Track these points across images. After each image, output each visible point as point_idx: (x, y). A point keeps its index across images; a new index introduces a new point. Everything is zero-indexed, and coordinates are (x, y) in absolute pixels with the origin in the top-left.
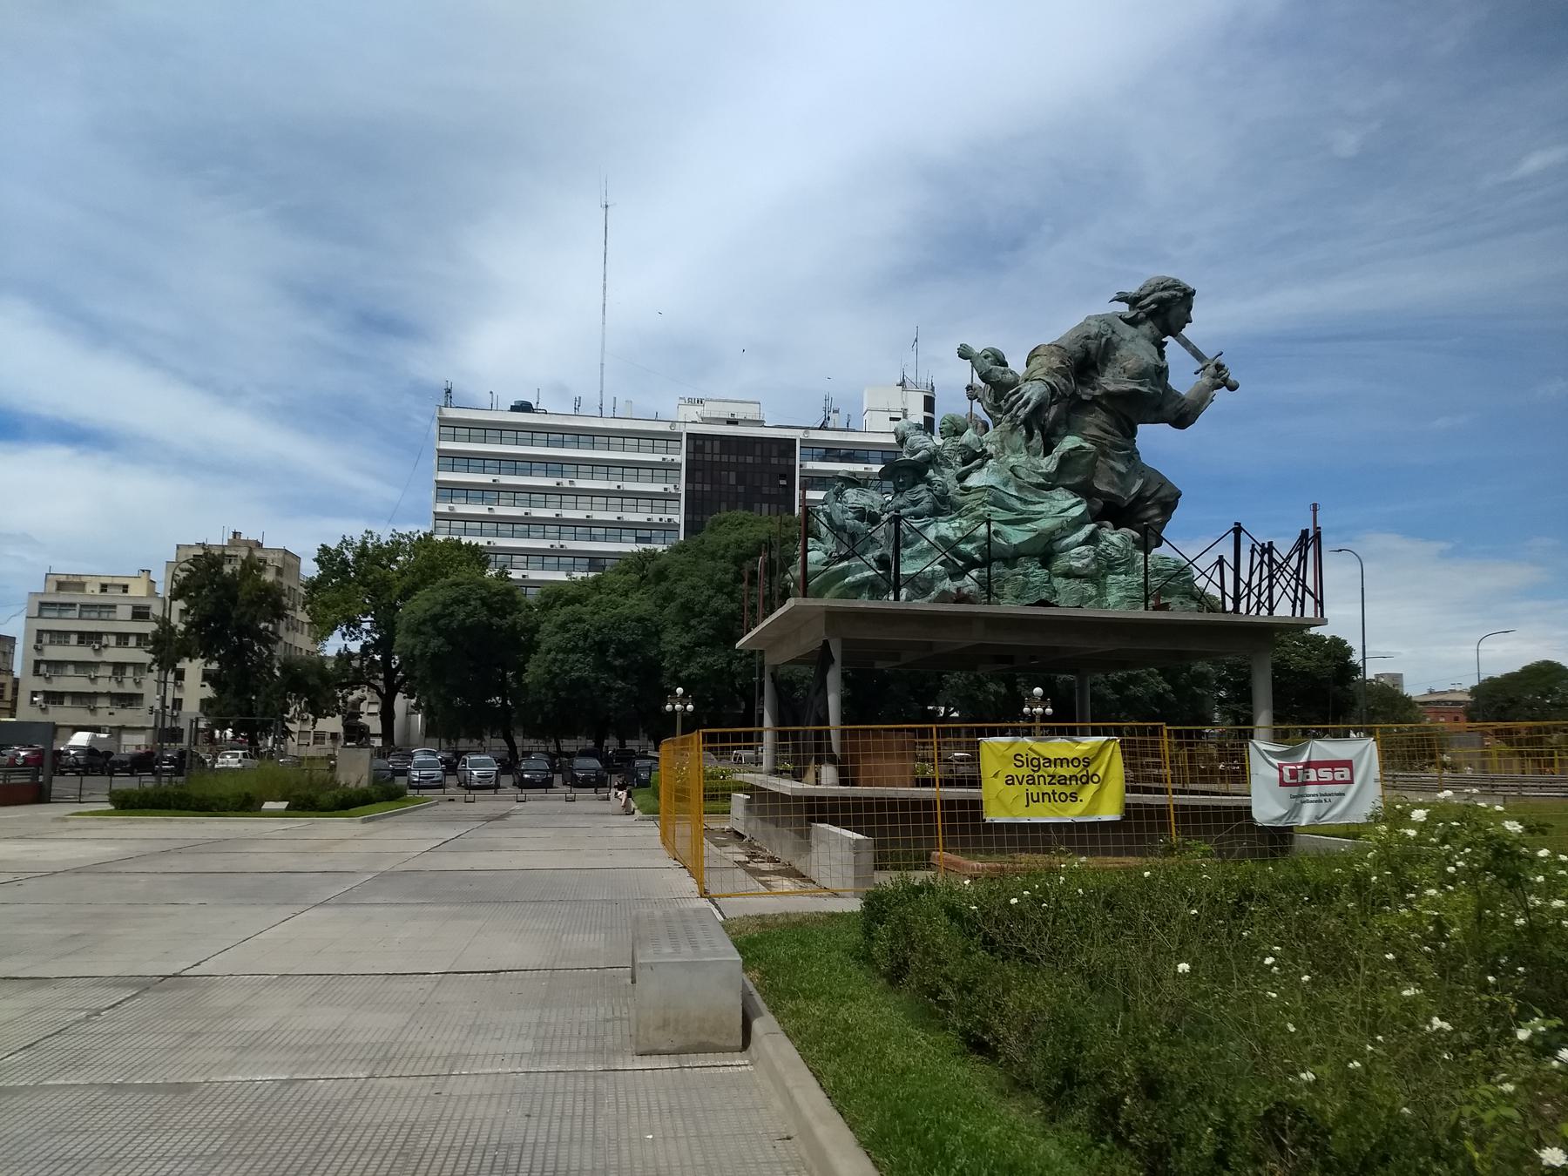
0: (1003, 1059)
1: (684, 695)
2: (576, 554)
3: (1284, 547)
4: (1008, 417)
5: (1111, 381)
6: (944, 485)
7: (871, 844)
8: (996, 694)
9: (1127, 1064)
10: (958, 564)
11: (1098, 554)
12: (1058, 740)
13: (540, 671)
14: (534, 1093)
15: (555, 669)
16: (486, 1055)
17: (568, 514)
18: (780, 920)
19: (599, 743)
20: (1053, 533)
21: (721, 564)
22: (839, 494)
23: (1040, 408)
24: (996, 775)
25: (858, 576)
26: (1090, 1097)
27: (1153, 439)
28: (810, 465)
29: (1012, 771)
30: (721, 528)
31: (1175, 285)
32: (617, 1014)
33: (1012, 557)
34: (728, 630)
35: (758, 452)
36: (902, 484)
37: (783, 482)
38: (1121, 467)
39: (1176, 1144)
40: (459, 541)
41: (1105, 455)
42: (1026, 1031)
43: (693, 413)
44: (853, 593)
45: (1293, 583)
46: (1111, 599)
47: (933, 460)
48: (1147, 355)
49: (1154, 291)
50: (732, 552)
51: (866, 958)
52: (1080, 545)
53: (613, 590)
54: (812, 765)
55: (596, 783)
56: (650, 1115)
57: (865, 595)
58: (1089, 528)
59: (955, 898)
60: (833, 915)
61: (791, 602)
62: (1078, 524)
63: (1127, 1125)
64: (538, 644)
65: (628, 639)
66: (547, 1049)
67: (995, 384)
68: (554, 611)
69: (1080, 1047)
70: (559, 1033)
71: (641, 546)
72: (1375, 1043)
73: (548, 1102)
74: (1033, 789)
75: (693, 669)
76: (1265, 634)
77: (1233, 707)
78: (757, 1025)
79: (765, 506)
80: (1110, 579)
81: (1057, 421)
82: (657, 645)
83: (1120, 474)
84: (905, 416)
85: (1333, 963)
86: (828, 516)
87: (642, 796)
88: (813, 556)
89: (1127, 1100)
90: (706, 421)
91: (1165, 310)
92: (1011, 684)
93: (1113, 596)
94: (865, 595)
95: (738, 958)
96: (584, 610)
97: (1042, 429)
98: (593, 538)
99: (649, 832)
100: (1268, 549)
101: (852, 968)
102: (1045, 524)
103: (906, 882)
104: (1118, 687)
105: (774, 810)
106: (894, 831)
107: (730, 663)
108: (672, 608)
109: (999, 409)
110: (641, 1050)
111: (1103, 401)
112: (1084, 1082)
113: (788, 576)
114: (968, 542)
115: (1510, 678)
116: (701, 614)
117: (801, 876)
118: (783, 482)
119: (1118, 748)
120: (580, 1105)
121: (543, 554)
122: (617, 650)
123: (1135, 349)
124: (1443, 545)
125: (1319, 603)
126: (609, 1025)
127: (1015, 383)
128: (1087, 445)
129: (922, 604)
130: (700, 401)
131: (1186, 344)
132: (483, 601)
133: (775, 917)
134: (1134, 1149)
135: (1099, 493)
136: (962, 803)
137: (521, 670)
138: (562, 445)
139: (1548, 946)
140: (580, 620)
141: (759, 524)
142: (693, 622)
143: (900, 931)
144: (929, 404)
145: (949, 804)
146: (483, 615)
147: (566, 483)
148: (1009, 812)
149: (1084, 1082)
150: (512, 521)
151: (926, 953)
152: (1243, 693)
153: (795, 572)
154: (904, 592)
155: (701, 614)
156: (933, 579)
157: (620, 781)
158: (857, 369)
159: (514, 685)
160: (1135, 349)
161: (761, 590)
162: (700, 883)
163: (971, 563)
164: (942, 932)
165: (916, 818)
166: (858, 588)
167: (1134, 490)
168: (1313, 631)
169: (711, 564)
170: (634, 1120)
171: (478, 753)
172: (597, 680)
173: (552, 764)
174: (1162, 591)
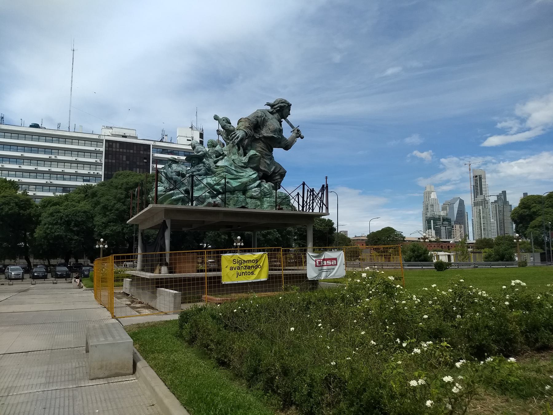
0: (232, 367)
1: (104, 242)
2: (57, 186)
3: (317, 190)
4: (231, 142)
5: (265, 132)
6: (209, 164)
7: (180, 294)
8: (224, 239)
9: (278, 365)
10: (214, 193)
11: (261, 191)
12: (248, 254)
13: (41, 232)
14: (47, 399)
15: (48, 231)
16: (24, 386)
17: (54, 169)
18: (146, 325)
19: (67, 261)
20: (247, 183)
21: (119, 191)
22: (170, 166)
23: (242, 140)
24: (227, 267)
25: (177, 196)
26: (263, 378)
27: (278, 153)
28: (156, 155)
29: (232, 265)
30: (120, 177)
31: (285, 102)
32: (81, 365)
33: (233, 191)
34: (122, 217)
35: (135, 149)
36: (194, 163)
37: (145, 161)
38: (268, 162)
39: (293, 391)
40: (6, 179)
41: (263, 157)
42: (241, 356)
43: (108, 132)
44: (175, 203)
45: (319, 202)
46: (265, 206)
47: (205, 155)
48: (276, 124)
49: (278, 103)
50: (124, 186)
51: (180, 336)
52: (255, 187)
53: (74, 200)
54: (158, 267)
55: (66, 276)
56: (97, 402)
57: (180, 203)
58: (258, 182)
59: (214, 311)
60: (167, 321)
61: (150, 206)
62: (255, 180)
63: (277, 386)
64: (40, 221)
65: (80, 220)
66: (51, 381)
67: (227, 130)
68: (48, 208)
69: (260, 360)
70: (56, 374)
71: (86, 183)
72: (355, 350)
73: (53, 402)
74: (239, 271)
75: (108, 231)
76: (311, 218)
77: (299, 242)
78: (139, 364)
79: (138, 170)
80: (265, 199)
81: (247, 145)
82: (92, 222)
83: (268, 164)
84: (193, 139)
85: (338, 325)
86: (166, 174)
87: (86, 281)
88: (160, 188)
89: (277, 378)
90: (113, 135)
91: (282, 110)
92: (229, 235)
93: (266, 205)
94: (180, 203)
95: (132, 340)
96: (61, 208)
97: (243, 147)
98: (64, 179)
99: (89, 295)
100: (312, 191)
101: (175, 340)
102: (244, 180)
103: (196, 307)
104: (264, 236)
105: (143, 284)
106: (189, 289)
107: (123, 229)
108: (98, 208)
109: (228, 139)
110: (92, 378)
111: (262, 137)
112: (261, 372)
113: (149, 196)
114: (218, 185)
115: (378, 232)
116: (111, 210)
117: (153, 308)
118: (145, 161)
119: (267, 259)
120: (67, 402)
121: (42, 185)
122: (75, 224)
123: (273, 122)
124: (361, 191)
125: (327, 208)
126: (77, 370)
127: (234, 131)
128: (258, 154)
129: (201, 207)
130: (111, 128)
131: (288, 122)
132: (17, 204)
133: (144, 324)
134: (279, 394)
135: (261, 170)
136: (214, 278)
137: (33, 232)
138: (52, 142)
139: (401, 315)
140: (59, 212)
141: (136, 176)
142: (107, 213)
143: (194, 325)
144: (201, 136)
145: (210, 278)
146: (16, 209)
147: (53, 157)
148: (231, 280)
149: (261, 372)
150: (29, 171)
151: (204, 332)
152: (303, 238)
153: (153, 194)
154: (194, 203)
155: (111, 210)
156: (205, 198)
157: (77, 275)
158: (177, 122)
159: (30, 238)
160: (273, 122)
161: (138, 201)
162: (112, 313)
163: (219, 193)
164: (210, 325)
165: (198, 284)
166: (177, 201)
167: (272, 170)
168: (323, 217)
169: (115, 191)
170: (90, 405)
171: (14, 265)
172: (66, 236)
173: (46, 269)
174: (281, 204)
